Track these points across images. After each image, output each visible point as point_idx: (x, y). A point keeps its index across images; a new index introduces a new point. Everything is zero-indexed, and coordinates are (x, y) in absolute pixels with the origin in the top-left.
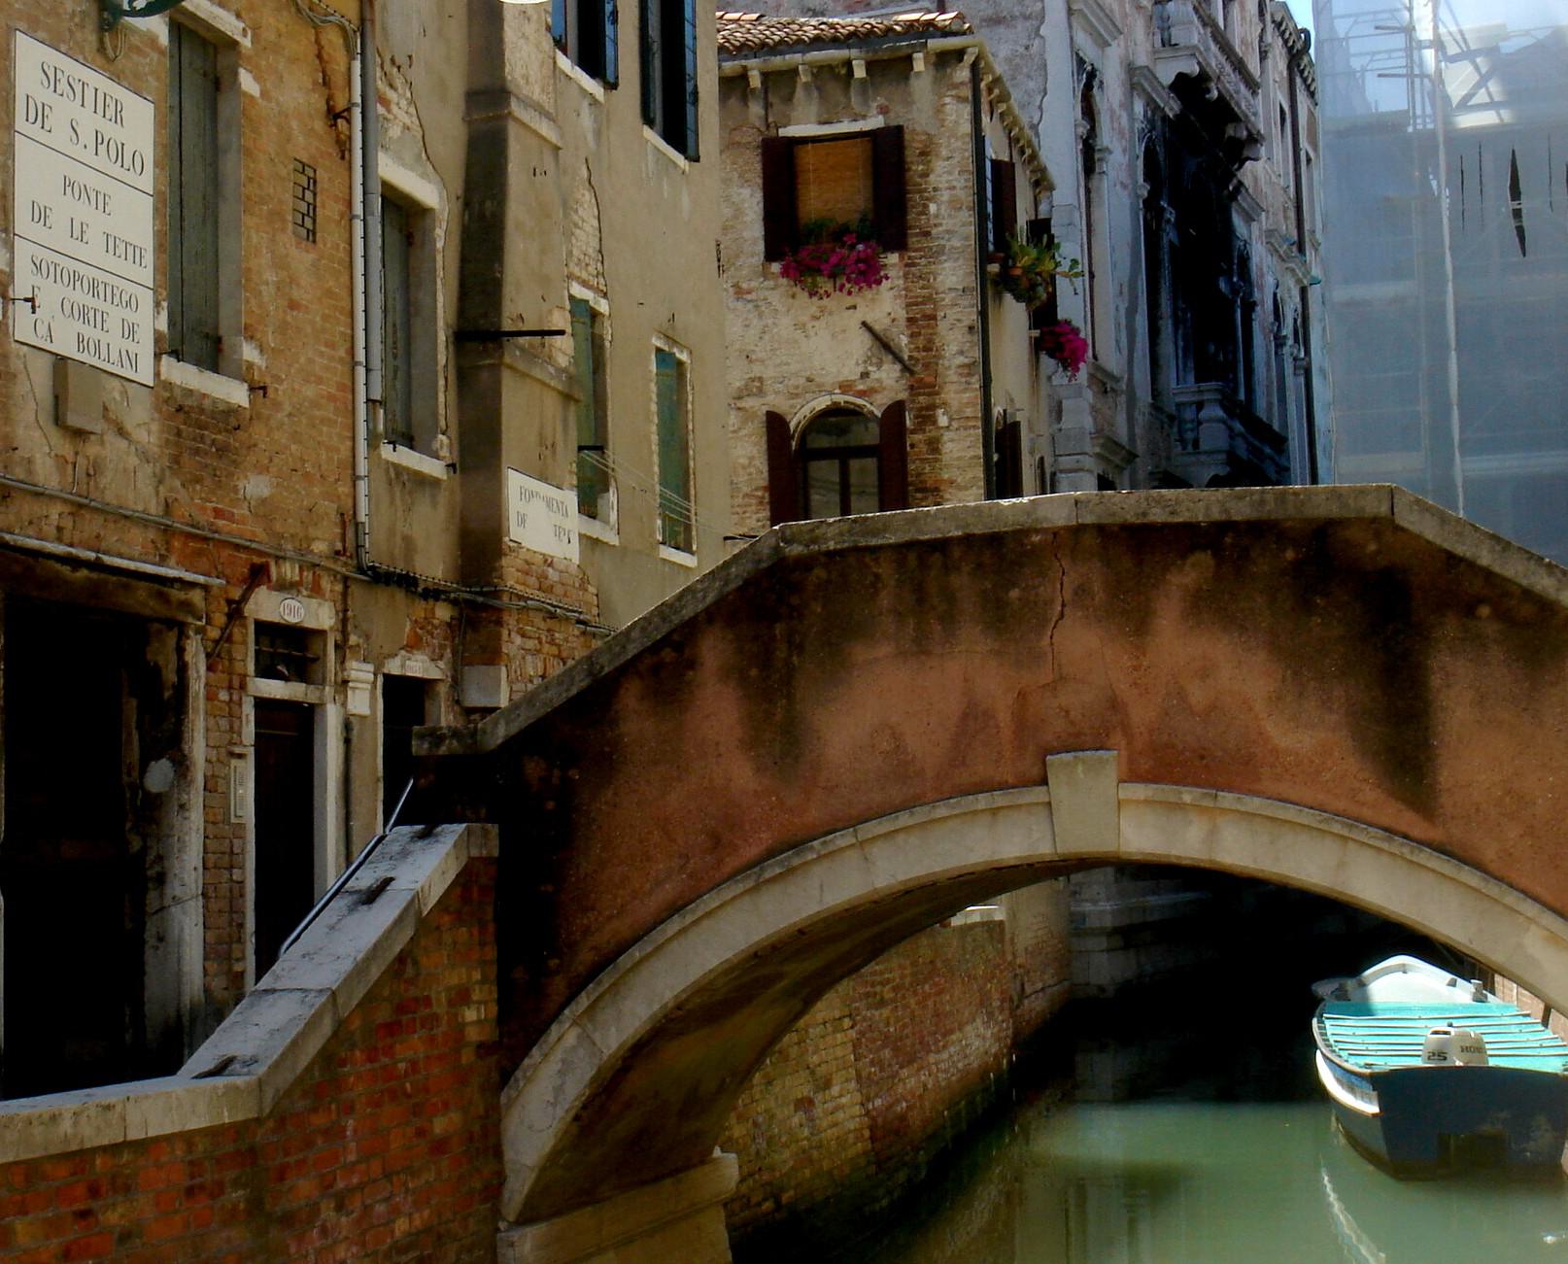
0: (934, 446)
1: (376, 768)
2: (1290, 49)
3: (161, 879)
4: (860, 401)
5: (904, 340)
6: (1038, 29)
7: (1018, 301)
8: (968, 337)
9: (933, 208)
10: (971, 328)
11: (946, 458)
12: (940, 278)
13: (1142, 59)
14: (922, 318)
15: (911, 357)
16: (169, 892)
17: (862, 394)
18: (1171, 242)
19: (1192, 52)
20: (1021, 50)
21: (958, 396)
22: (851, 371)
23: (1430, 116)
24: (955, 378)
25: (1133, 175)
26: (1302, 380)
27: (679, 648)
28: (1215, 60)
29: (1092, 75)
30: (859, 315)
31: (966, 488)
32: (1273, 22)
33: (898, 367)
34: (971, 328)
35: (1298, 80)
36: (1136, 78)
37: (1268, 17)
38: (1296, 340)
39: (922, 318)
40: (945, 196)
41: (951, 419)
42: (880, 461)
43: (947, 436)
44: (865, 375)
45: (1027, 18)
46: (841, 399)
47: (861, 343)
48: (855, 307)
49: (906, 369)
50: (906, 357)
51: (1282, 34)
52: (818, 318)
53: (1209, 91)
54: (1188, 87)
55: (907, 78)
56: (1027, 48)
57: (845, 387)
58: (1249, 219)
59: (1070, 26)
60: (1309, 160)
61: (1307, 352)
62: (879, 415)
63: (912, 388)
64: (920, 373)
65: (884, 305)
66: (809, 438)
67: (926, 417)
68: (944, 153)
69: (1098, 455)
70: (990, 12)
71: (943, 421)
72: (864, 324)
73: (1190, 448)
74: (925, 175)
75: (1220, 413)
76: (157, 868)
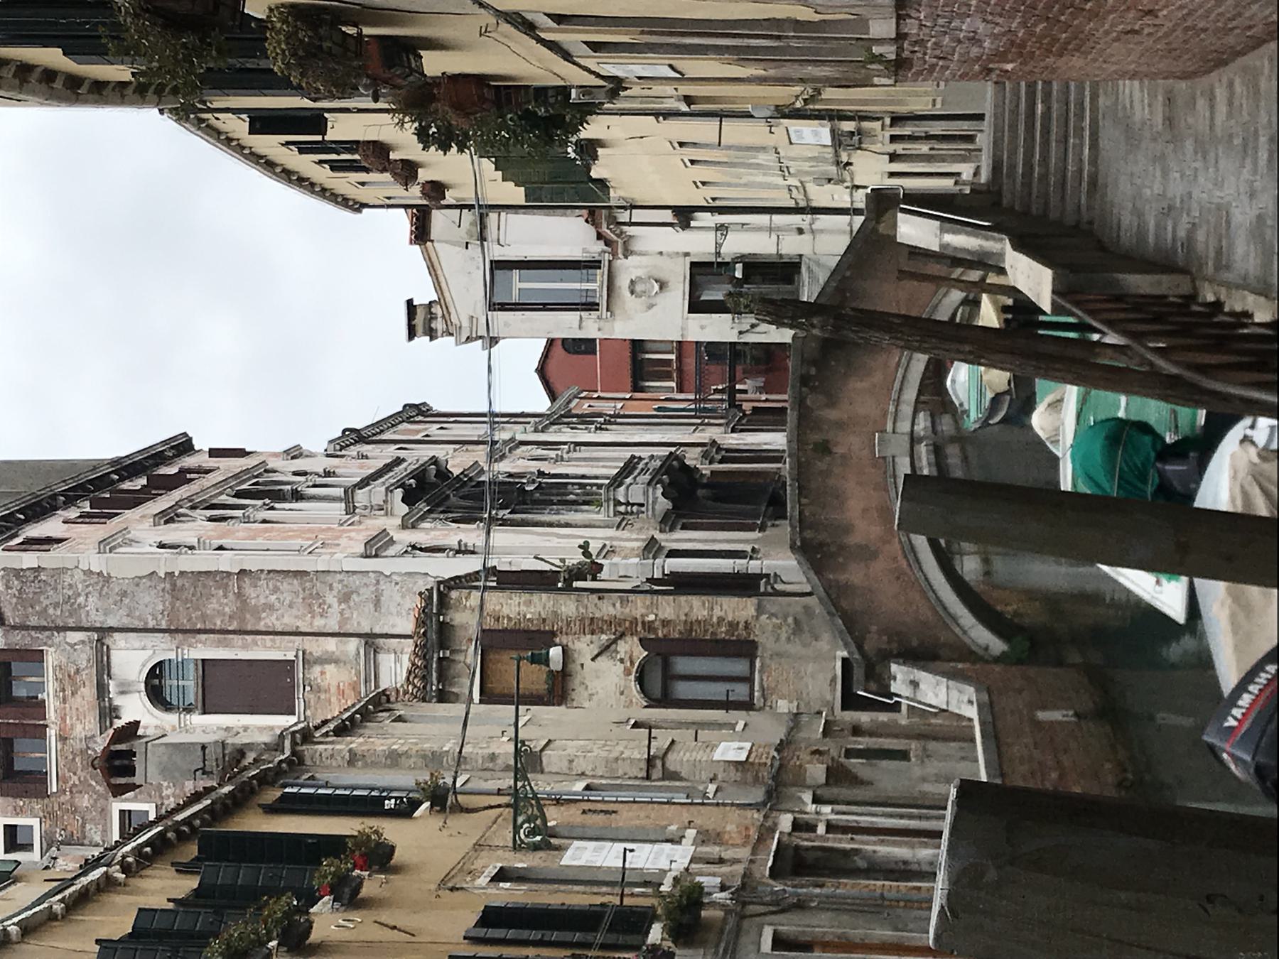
0: (665, 623)
1: (862, 764)
2: (356, 442)
3: (905, 862)
4: (637, 665)
5: (604, 637)
6: (386, 576)
7: (1015, 250)
8: (605, 601)
9: (529, 616)
10: (600, 598)
11: (672, 617)
12: (570, 614)
13: (399, 521)
14: (592, 626)
15: (614, 634)
16: (910, 860)
17: (632, 663)
18: (760, 390)
19: (389, 490)
20: (398, 587)
21: (639, 607)
22: (620, 668)
23: (983, 279)
24: (628, 610)
25: (471, 530)
26: (583, 448)
27: (830, 587)
28: (391, 478)
29: (414, 547)
30: (588, 663)
31: (691, 607)
32: (341, 450)
33: (619, 642)
34: (600, 598)
35: (378, 437)
36: (408, 524)
37: (339, 453)
38: (558, 449)
39: (592, 626)
40: (523, 608)
41: (652, 613)
42: (675, 654)
43: (661, 616)
44: (622, 661)
45: (378, 582)
46: (632, 677)
47: (603, 662)
48: (582, 665)
49: (622, 636)
50: (613, 637)
51: (348, 446)
52: (587, 687)
53: (411, 485)
54: (410, 498)
55: (453, 626)
56: (397, 584)
57: (627, 672)
58: (482, 472)
59: (386, 557)
60: (427, 436)
61: (565, 443)
62: (646, 653)
63: (632, 634)
64: (621, 629)
65: (584, 647)
66: (654, 697)
67: (649, 626)
68: (498, 608)
69: (654, 558)
70: (372, 606)
71: (652, 617)
72: (593, 659)
73: (643, 509)
74: (510, 619)
75: (622, 489)
76: (901, 864)
